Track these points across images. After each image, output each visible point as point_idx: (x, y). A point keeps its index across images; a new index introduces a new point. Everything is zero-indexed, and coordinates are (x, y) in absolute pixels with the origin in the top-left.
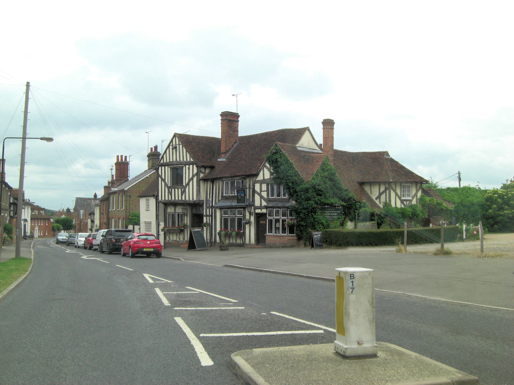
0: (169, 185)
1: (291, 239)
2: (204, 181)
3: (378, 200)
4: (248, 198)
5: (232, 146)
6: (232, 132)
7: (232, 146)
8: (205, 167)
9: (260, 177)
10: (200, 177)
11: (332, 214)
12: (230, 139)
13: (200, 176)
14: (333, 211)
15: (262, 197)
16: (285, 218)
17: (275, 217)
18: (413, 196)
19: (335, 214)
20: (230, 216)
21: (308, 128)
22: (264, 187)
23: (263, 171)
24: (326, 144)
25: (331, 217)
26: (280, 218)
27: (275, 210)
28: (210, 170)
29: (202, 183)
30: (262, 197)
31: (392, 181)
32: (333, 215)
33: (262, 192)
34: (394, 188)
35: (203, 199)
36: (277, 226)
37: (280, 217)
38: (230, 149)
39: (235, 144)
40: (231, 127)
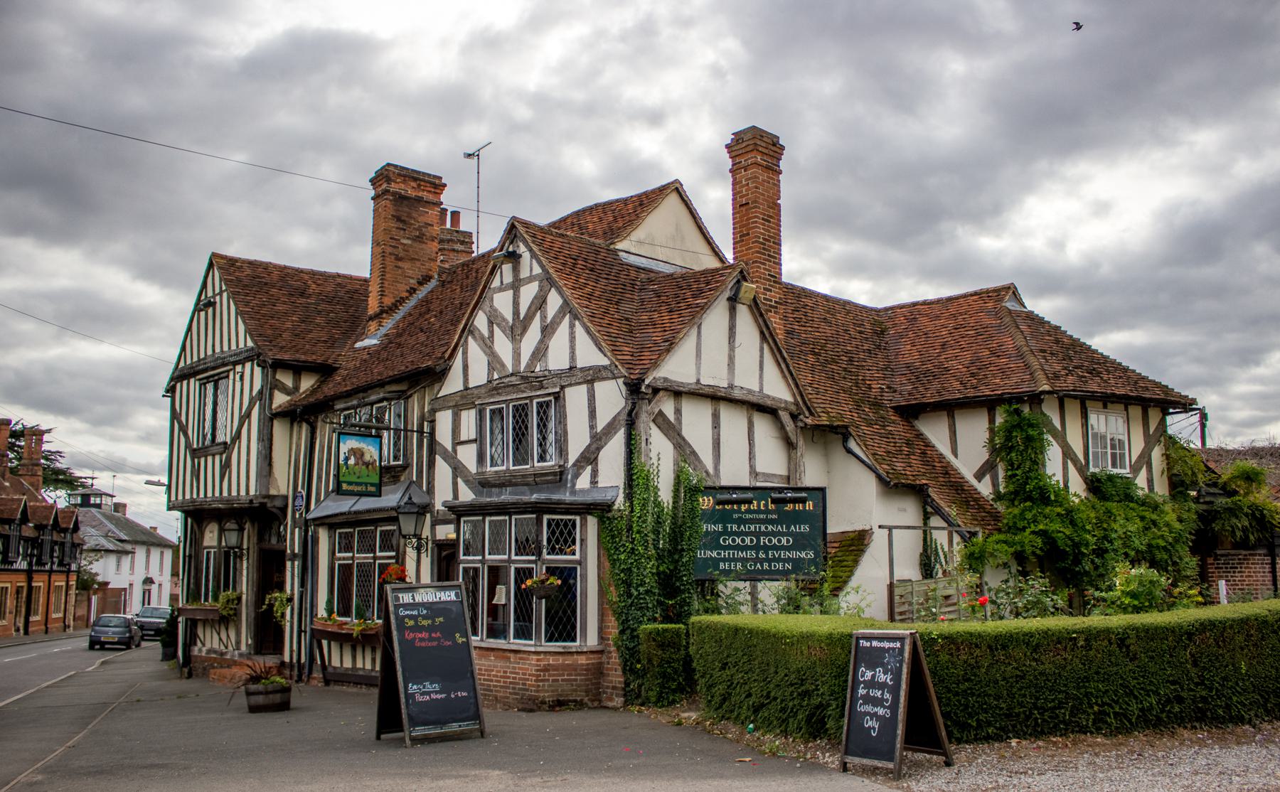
0: (195, 446)
1: (555, 668)
2: (288, 420)
3: (987, 478)
4: (415, 479)
5: (407, 291)
6: (409, 242)
7: (407, 291)
8: (298, 369)
9: (453, 384)
10: (274, 406)
11: (770, 541)
12: (400, 264)
13: (271, 403)
14: (770, 527)
15: (458, 470)
16: (530, 562)
17: (488, 557)
18: (1136, 462)
19: (784, 541)
20: (358, 558)
21: (678, 185)
22: (469, 419)
23: (465, 353)
24: (748, 234)
25: (761, 555)
26: (510, 561)
27: (490, 522)
28: (316, 382)
29: (280, 430)
30: (458, 470)
31: (1046, 388)
32: (775, 548)
33: (459, 448)
34: (1057, 423)
35: (283, 491)
36: (500, 599)
37: (506, 557)
38: (402, 301)
39: (421, 283)
40: (403, 222)
